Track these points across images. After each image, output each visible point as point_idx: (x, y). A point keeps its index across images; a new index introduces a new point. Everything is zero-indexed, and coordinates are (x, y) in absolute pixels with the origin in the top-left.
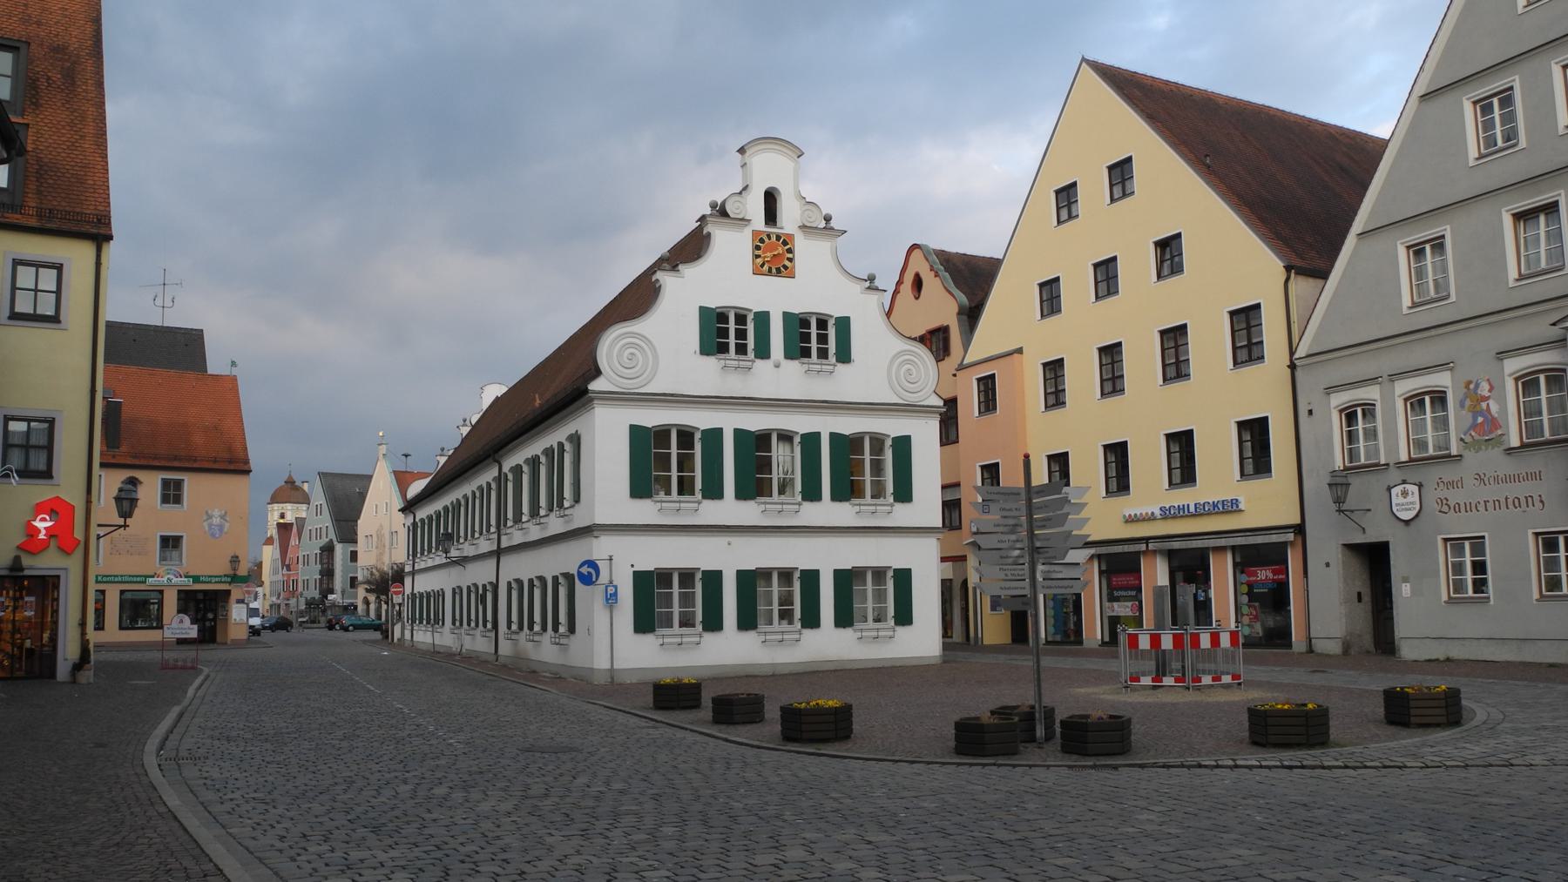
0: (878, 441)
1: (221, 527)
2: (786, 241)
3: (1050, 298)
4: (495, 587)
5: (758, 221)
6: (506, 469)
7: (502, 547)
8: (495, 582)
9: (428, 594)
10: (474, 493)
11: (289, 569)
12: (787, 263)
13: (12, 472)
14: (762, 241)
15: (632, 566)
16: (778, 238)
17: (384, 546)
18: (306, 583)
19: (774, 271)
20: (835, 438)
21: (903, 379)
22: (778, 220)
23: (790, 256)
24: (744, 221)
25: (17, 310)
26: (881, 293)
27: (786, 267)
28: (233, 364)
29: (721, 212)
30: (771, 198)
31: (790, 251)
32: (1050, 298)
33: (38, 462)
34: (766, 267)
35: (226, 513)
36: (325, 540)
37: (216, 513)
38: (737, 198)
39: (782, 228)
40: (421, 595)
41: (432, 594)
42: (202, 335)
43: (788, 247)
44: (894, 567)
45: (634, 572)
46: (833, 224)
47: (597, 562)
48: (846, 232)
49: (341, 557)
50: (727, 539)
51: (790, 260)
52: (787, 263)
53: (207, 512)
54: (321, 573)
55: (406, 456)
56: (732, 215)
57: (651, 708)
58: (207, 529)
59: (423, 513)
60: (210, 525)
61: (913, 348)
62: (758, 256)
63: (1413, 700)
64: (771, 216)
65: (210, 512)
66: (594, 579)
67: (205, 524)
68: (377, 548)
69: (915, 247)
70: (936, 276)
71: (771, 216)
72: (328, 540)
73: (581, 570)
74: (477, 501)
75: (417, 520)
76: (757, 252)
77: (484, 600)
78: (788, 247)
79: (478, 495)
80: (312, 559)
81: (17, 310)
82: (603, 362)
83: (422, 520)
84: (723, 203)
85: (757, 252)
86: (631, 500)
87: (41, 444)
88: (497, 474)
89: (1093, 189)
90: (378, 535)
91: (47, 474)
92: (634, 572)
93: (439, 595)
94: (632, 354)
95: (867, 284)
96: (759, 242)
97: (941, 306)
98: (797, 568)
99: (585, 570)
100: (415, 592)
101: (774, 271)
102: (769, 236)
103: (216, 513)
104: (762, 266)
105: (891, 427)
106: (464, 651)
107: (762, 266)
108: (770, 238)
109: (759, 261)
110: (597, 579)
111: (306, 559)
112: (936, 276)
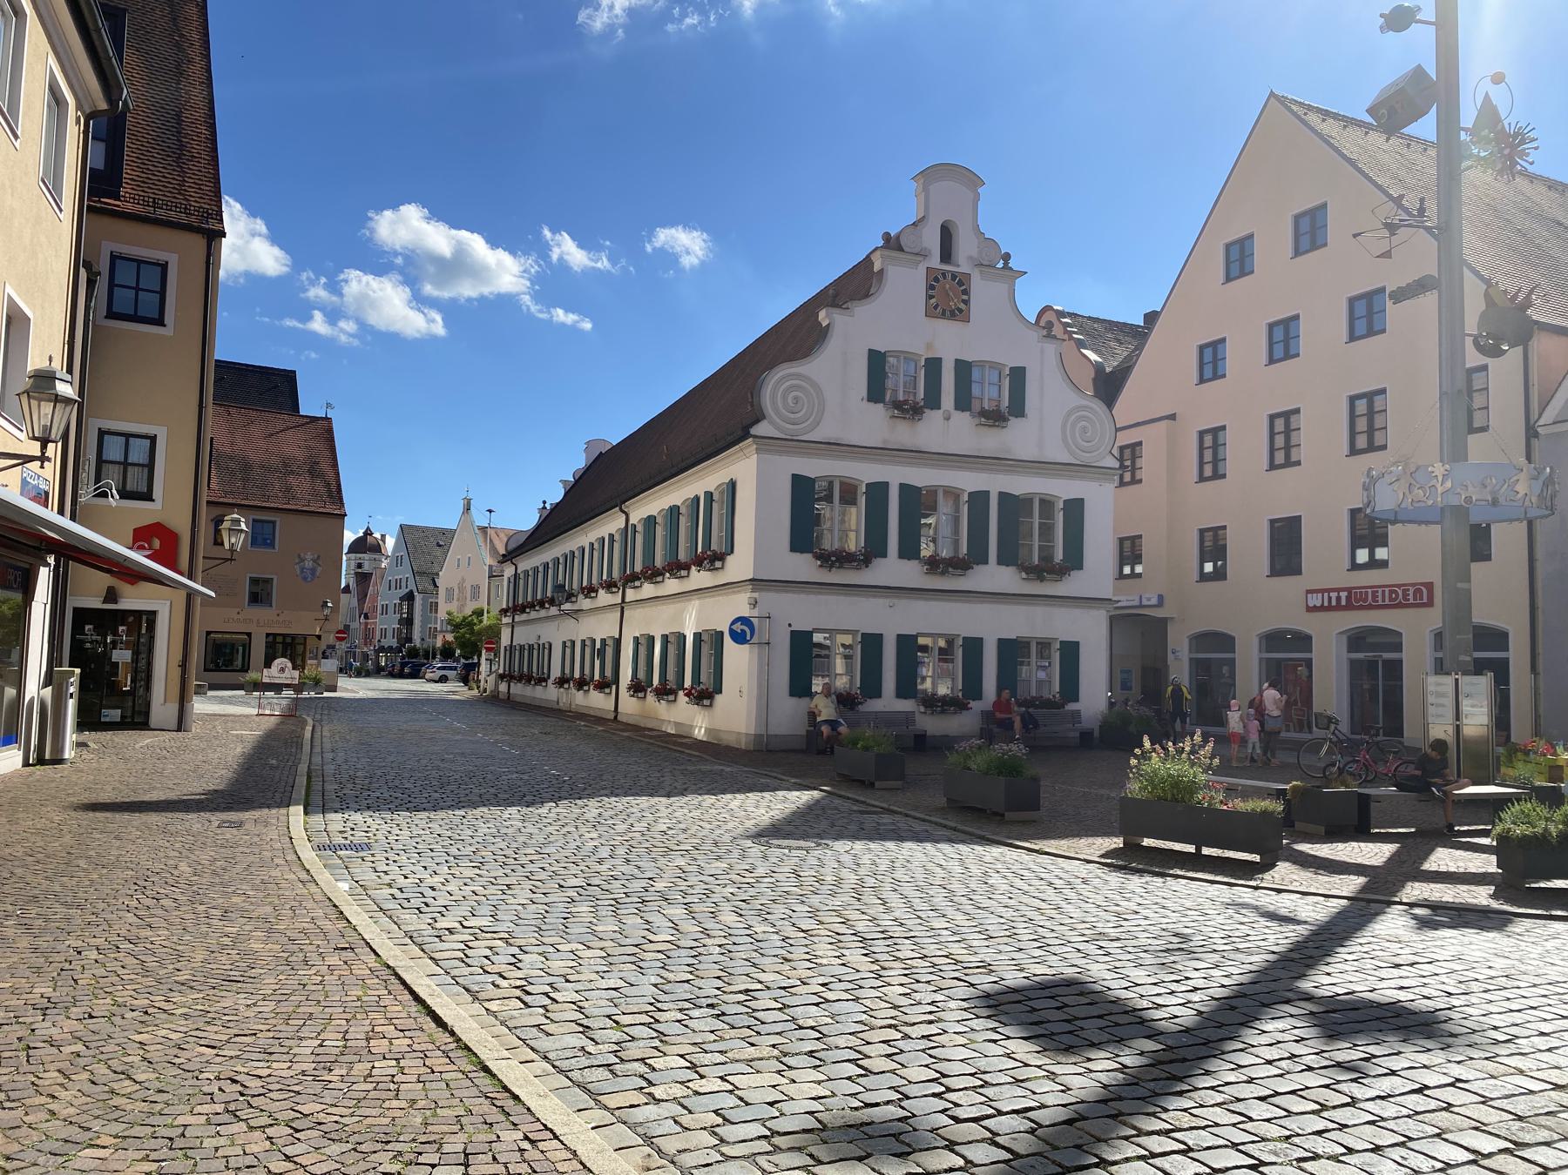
0: (1047, 504)
1: (313, 571)
2: (962, 282)
3: (1211, 360)
4: (618, 642)
5: (935, 261)
6: (634, 520)
7: (627, 600)
9: (531, 647)
10: (592, 545)
11: (366, 617)
12: (962, 306)
13: (111, 490)
14: (936, 280)
15: (790, 625)
16: (954, 277)
18: (384, 633)
20: (1004, 497)
23: (965, 297)
24: (923, 254)
25: (114, 310)
26: (1059, 342)
27: (961, 311)
29: (892, 243)
30: (947, 234)
31: (966, 292)
32: (1211, 360)
33: (135, 481)
35: (319, 557)
36: (405, 591)
37: (309, 556)
39: (958, 266)
40: (522, 647)
43: (964, 287)
48: (1026, 273)
51: (966, 302)
52: (962, 306)
53: (299, 556)
54: (400, 622)
55: (490, 511)
56: (906, 249)
57: (943, 808)
58: (298, 572)
59: (527, 563)
60: (302, 570)
61: (1090, 404)
62: (931, 297)
64: (947, 254)
65: (302, 555)
66: (748, 638)
67: (297, 567)
68: (458, 600)
71: (947, 254)
72: (408, 590)
73: (734, 627)
74: (595, 553)
75: (519, 571)
77: (602, 653)
78: (964, 287)
79: (596, 546)
80: (391, 609)
81: (114, 310)
83: (526, 572)
84: (898, 237)
87: (141, 462)
88: (623, 526)
89: (1273, 246)
91: (148, 496)
93: (544, 648)
95: (1045, 332)
96: (934, 280)
97: (991, 392)
98: (959, 635)
99: (738, 627)
102: (944, 275)
103: (309, 556)
104: (936, 307)
105: (1062, 489)
107: (936, 307)
108: (945, 278)
109: (933, 301)
110: (751, 638)
111: (385, 609)
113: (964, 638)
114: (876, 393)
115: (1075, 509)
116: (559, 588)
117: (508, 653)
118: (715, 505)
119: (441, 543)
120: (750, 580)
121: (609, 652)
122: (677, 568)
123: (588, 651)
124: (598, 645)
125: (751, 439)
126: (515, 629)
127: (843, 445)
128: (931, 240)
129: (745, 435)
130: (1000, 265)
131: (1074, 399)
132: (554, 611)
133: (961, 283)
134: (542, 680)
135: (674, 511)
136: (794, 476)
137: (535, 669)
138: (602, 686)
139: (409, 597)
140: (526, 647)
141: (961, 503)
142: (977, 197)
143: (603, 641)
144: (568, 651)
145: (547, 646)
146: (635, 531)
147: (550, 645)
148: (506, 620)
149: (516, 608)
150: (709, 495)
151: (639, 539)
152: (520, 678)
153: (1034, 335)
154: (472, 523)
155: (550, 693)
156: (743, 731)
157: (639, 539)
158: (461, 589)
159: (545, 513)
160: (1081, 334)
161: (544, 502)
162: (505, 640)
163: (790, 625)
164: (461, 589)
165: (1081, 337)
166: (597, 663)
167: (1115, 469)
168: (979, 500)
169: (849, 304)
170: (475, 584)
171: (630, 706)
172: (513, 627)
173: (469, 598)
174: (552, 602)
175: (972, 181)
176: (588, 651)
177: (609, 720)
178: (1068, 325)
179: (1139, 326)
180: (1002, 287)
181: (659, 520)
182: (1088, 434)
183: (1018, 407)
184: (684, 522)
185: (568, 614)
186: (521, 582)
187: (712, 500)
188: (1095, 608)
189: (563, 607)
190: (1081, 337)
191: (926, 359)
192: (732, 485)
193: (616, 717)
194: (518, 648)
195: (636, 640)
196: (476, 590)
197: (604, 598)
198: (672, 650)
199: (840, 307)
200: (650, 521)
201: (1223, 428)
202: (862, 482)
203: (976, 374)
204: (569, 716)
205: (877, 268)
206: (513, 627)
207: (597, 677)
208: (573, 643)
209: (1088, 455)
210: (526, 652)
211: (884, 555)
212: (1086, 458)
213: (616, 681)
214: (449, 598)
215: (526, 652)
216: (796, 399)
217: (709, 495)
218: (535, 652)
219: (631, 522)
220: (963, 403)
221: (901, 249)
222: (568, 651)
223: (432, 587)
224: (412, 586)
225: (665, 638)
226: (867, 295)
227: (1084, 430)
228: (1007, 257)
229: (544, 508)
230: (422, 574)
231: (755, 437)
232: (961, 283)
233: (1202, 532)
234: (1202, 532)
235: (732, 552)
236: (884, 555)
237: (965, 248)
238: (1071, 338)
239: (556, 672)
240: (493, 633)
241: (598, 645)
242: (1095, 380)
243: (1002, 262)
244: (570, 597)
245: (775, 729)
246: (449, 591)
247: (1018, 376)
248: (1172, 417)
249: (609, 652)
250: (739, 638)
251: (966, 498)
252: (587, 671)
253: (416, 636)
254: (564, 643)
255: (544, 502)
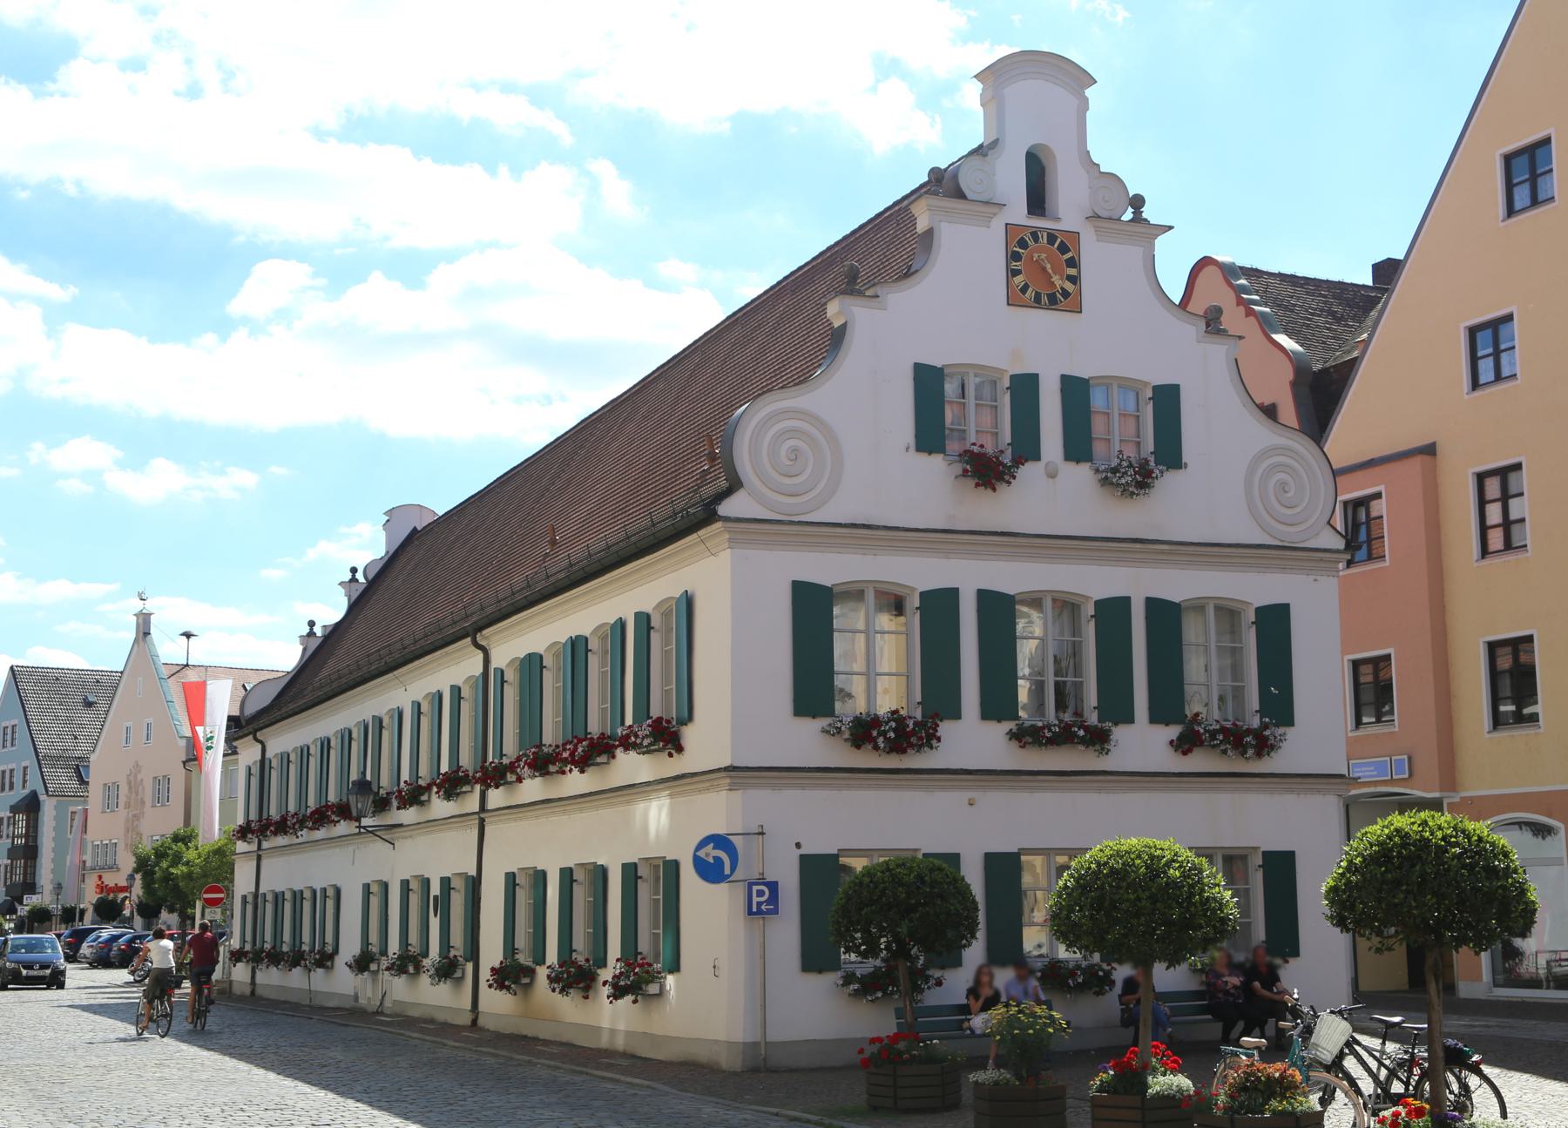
2: (1065, 247)
4: (474, 885)
5: (1018, 212)
8: (473, 872)
9: (297, 897)
10: (417, 706)
12: (1069, 286)
15: (798, 845)
16: (1052, 238)
17: (143, 802)
19: (1045, 299)
21: (1273, 499)
22: (1046, 205)
23: (1072, 272)
27: (1066, 294)
28: (907, 449)
29: (943, 184)
31: (1072, 263)
34: (1030, 293)
36: (19, 793)
38: (976, 160)
40: (278, 898)
41: (307, 894)
42: (1179, 388)
43: (1069, 255)
44: (1263, 849)
45: (802, 857)
46: (1147, 213)
47: (730, 837)
48: (1171, 228)
49: (53, 834)
50: (966, 795)
51: (1074, 280)
52: (1069, 286)
55: (188, 635)
56: (969, 197)
59: (285, 740)
61: (1300, 448)
62: (1015, 273)
63: (1369, 674)
64: (1037, 201)
66: (727, 871)
68: (128, 806)
69: (1205, 262)
70: (1247, 316)
71: (1037, 201)
72: (27, 791)
73: (701, 854)
75: (269, 755)
76: (1015, 265)
78: (1069, 255)
82: (744, 464)
83: (285, 758)
85: (1015, 265)
86: (982, 721)
88: (479, 670)
90: (129, 783)
92: (802, 857)
94: (795, 450)
96: (1018, 246)
98: (1256, 849)
99: (710, 853)
100: (262, 890)
101: (1045, 299)
104: (1024, 290)
106: (388, 1004)
107: (1024, 290)
108: (1036, 239)
109: (1019, 279)
110: (733, 869)
112: (1247, 316)
113: (1264, 853)
114: (929, 436)
115: (1274, 622)
116: (363, 786)
117: (249, 908)
118: (655, 639)
119: (91, 699)
120: (726, 769)
121: (458, 902)
122: (595, 751)
123: (414, 900)
124: (435, 890)
125: (718, 525)
126: (264, 862)
127: (877, 528)
128: (1011, 182)
129: (708, 515)
130: (1128, 215)
131: (1263, 434)
132: (344, 827)
133: (1063, 249)
134: (325, 960)
135: (578, 647)
136: (794, 583)
137: (306, 937)
138: (447, 970)
139: (31, 806)
140: (288, 896)
141: (1083, 620)
142: (1084, 105)
143: (446, 883)
144: (375, 902)
145: (330, 892)
146: (503, 682)
147: (338, 892)
148: (241, 846)
149: (258, 829)
150: (643, 620)
151: (511, 694)
152: (275, 958)
153: (1191, 331)
154: (153, 657)
155: (341, 982)
156: (722, 1037)
157: (511, 694)
158: (134, 785)
159: (314, 644)
160: (1266, 305)
161: (312, 624)
162: (243, 881)
163: (798, 845)
164: (134, 785)
165: (1268, 310)
166: (435, 923)
167: (1338, 551)
168: (1113, 612)
169: (878, 290)
170: (160, 774)
171: (497, 1004)
172: (259, 858)
173: (148, 802)
174: (344, 811)
175: (1077, 78)
176: (414, 900)
177: (463, 1028)
178: (1244, 289)
179: (1364, 286)
180: (1135, 252)
181: (547, 662)
182: (1289, 495)
183: (1170, 452)
184: (596, 667)
185: (372, 832)
186: (274, 774)
187: (649, 628)
188: (1319, 791)
189: (365, 822)
190: (1268, 310)
191: (1012, 377)
192: (688, 603)
193: (475, 1022)
194: (270, 897)
195: (511, 879)
196: (162, 784)
197: (440, 807)
198: (581, 895)
199: (861, 294)
200: (532, 665)
201: (1517, 467)
202: (913, 589)
203: (1097, 400)
204: (382, 1023)
205: (922, 225)
206: (259, 858)
207: (394, 946)
208: (385, 886)
209: (1291, 529)
210: (288, 907)
211: (956, 715)
212: (1290, 535)
213: (473, 953)
214: (111, 801)
215: (288, 907)
216: (795, 454)
217: (456, 691)
218: (307, 906)
219: (494, 665)
220: (1078, 447)
221: (960, 195)
222: (375, 902)
223: (75, 784)
224: (34, 783)
225: (567, 875)
226: (908, 274)
227: (1283, 487)
228: (1138, 202)
229: (311, 634)
230: (56, 760)
231: (727, 519)
232: (1063, 249)
233: (1492, 647)
234: (1492, 647)
235: (690, 718)
236: (956, 715)
237: (1069, 210)
238: (1250, 313)
239: (350, 947)
240: (219, 867)
241: (435, 890)
242: (1294, 385)
243: (1130, 210)
244: (382, 805)
245: (775, 1035)
246: (110, 790)
247: (1167, 400)
248: (1430, 450)
249: (458, 902)
250: (710, 872)
251: (1091, 610)
252: (414, 938)
253: (45, 875)
254: (367, 887)
255: (312, 624)
